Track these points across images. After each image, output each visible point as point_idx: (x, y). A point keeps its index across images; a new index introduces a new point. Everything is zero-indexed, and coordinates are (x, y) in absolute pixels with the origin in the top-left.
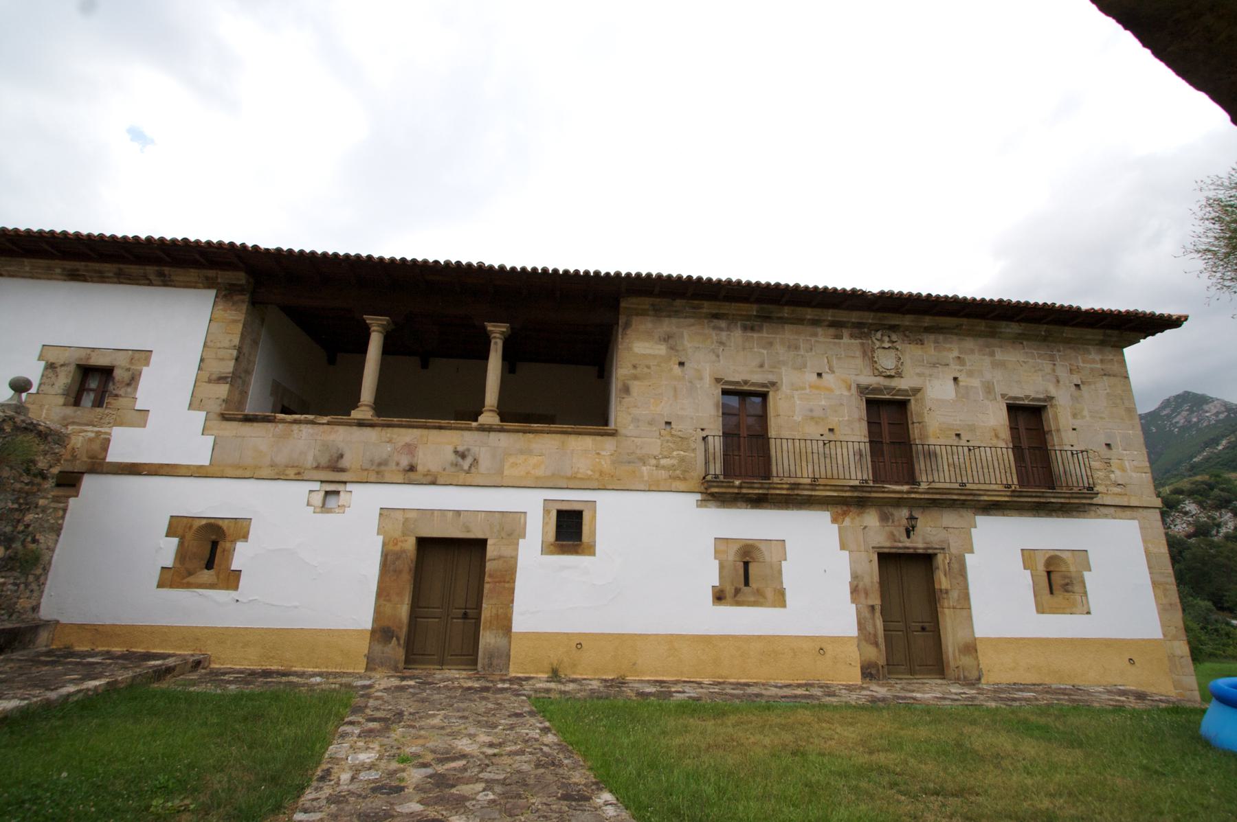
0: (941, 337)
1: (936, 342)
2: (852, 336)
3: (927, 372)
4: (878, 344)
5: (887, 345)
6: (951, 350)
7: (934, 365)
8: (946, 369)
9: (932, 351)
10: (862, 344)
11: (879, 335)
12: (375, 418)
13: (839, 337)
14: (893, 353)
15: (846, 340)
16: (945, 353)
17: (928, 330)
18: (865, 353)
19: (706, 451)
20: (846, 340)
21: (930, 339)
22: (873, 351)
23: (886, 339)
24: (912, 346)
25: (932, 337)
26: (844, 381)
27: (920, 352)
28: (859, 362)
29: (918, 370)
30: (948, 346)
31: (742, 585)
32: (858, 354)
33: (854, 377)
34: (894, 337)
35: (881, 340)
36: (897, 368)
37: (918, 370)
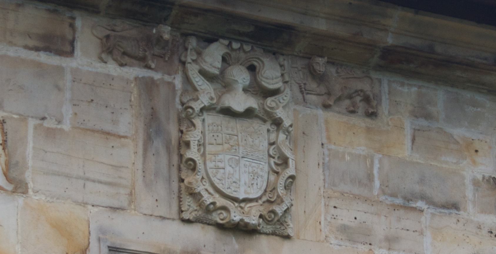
0: (439, 97)
1: (422, 112)
2: (109, 49)
3: (381, 225)
4: (207, 93)
5: (239, 101)
6: (470, 149)
7: (407, 202)
8: (448, 221)
9: (405, 150)
10: (148, 87)
11: (213, 56)
12: (180, 72)
13: (58, 44)
14: (259, 136)
15: (85, 60)
16: (448, 161)
17: (398, 62)
18: (153, 125)
19: (100, 182)
20: (85, 60)
21: (399, 95)
22: (186, 119)
23: (240, 76)
24: (335, 119)
25: (409, 92)
26: (61, 228)
27: (360, 146)
28: (128, 155)
29: (346, 216)
30: (459, 132)
31: (242, 211)
32: (128, 122)
33: (98, 218)
34: (271, 74)
35: (219, 80)
36: (270, 197)
37: (346, 216)
